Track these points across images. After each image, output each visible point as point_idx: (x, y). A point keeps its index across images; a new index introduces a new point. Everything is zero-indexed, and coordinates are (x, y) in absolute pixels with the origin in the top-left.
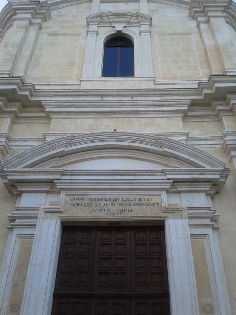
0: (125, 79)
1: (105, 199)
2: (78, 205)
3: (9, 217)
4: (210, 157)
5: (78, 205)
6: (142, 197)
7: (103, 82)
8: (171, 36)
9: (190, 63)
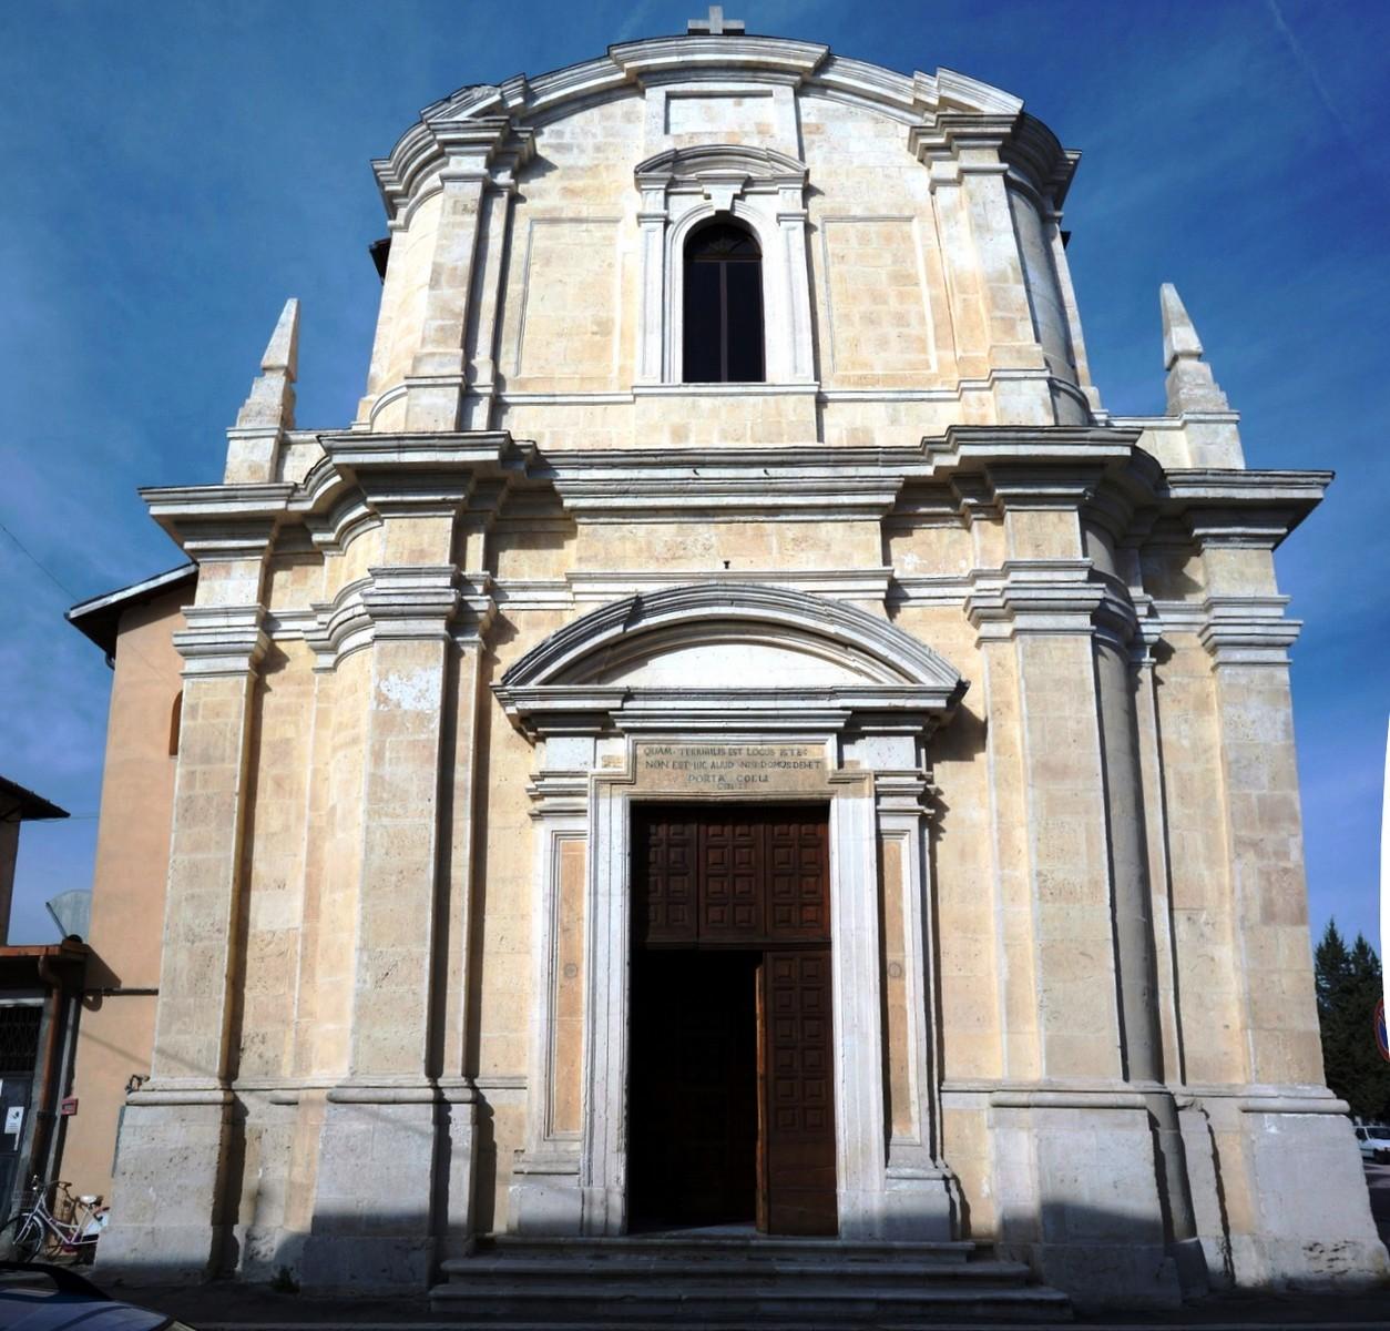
1: (712, 752)
2: (660, 764)
3: (529, 790)
4: (932, 656)
5: (660, 764)
6: (786, 747)
7: (691, 399)
9: (908, 325)
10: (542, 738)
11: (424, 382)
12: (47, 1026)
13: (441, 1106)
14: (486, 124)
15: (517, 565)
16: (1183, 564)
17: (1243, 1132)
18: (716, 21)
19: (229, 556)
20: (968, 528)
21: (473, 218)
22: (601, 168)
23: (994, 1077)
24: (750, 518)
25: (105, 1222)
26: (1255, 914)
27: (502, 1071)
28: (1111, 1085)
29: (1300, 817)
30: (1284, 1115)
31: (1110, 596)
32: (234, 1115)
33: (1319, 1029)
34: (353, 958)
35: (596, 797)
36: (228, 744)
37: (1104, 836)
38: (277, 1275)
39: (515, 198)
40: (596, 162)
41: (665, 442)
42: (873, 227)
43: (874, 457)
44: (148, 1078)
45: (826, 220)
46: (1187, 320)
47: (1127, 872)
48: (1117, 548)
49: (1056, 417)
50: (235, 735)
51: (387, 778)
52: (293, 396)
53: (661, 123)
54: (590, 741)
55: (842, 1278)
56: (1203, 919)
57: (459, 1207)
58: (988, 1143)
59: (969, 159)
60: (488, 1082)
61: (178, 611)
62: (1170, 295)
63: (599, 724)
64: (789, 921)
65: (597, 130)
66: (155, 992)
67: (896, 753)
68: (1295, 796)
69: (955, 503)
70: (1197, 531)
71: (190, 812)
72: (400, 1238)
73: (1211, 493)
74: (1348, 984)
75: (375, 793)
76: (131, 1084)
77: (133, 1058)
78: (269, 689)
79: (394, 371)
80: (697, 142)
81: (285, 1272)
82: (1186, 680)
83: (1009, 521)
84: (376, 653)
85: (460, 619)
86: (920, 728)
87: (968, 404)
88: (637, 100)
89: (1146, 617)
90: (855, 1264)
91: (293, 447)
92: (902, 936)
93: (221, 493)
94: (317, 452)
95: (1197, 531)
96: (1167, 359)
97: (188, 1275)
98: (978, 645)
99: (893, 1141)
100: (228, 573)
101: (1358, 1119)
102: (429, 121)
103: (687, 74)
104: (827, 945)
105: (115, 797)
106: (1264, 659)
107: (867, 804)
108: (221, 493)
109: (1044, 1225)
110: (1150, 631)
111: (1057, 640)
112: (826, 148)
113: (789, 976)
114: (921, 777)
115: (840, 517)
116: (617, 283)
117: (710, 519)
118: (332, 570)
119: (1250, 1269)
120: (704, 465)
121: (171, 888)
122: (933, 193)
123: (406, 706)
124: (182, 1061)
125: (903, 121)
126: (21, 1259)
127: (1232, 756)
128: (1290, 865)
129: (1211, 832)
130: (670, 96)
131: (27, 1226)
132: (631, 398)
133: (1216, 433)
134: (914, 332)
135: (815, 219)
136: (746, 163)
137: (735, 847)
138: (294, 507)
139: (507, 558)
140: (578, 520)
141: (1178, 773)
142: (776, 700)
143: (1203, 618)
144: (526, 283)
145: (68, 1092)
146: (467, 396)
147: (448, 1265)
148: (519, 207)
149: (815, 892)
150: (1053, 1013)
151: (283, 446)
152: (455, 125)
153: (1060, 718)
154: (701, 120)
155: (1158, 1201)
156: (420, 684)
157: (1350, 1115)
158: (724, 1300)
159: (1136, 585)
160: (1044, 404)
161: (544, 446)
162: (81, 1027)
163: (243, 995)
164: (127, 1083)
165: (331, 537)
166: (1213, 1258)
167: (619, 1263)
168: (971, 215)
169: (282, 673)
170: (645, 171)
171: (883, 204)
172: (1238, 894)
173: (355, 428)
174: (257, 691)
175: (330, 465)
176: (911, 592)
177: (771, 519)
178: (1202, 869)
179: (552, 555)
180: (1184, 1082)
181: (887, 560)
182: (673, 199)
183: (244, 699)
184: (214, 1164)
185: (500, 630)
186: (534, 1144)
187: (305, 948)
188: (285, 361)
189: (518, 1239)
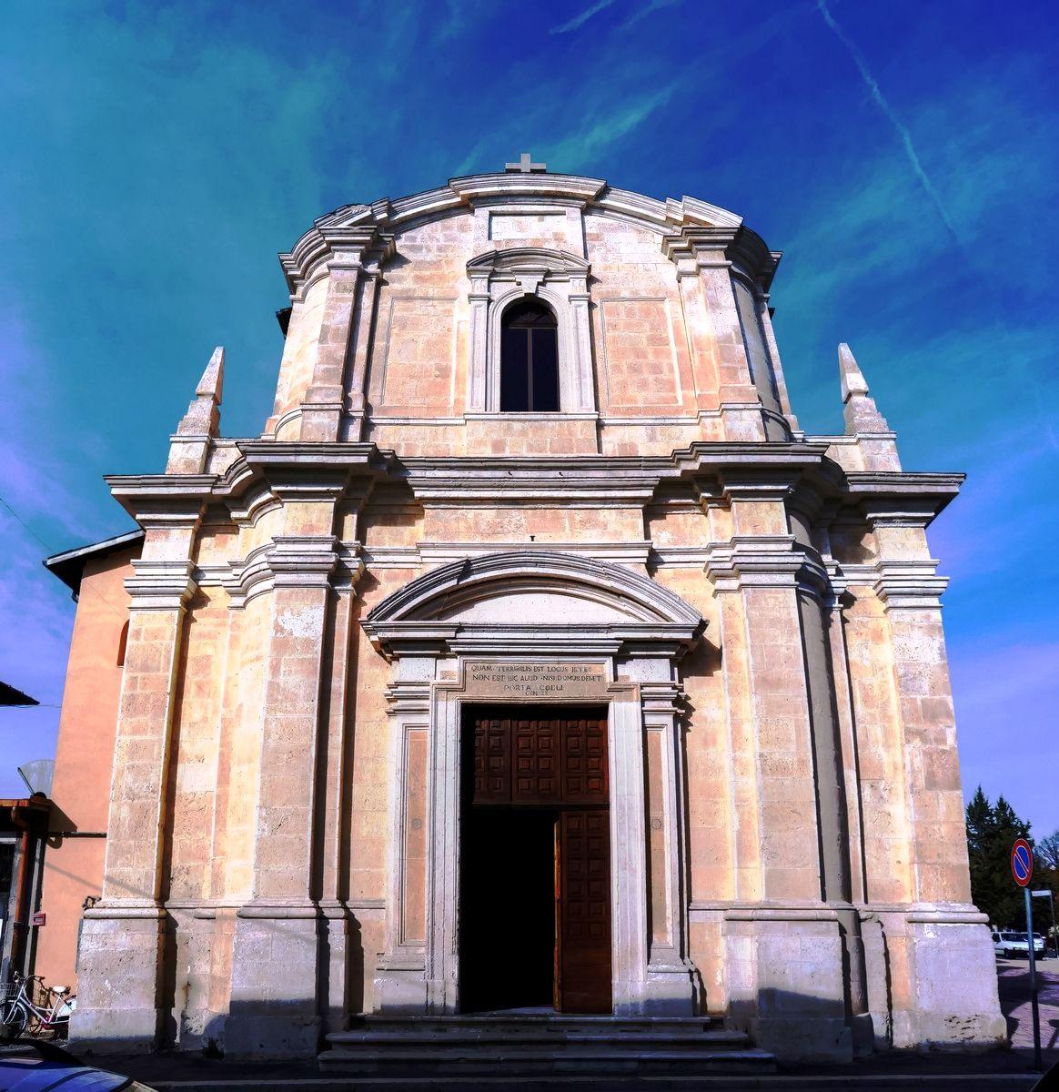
0: (545, 417)
1: (522, 669)
2: (484, 677)
3: (386, 695)
5: (484, 677)
7: (505, 423)
8: (627, 303)
10: (396, 658)
11: (314, 407)
12: (18, 859)
13: (322, 921)
14: (360, 231)
15: (380, 537)
16: (860, 538)
17: (909, 937)
18: (526, 163)
19: (168, 525)
20: (706, 514)
21: (351, 295)
22: (443, 263)
23: (727, 899)
24: (549, 506)
25: (74, 1006)
26: (921, 782)
27: (366, 896)
28: (813, 904)
29: (953, 713)
30: (939, 924)
31: (809, 561)
32: (168, 928)
33: (968, 863)
34: (255, 813)
35: (436, 700)
36: (162, 658)
37: (809, 728)
38: (206, 1045)
39: (381, 283)
40: (438, 258)
41: (488, 452)
42: (637, 305)
43: (638, 464)
44: (100, 899)
45: (606, 299)
46: (857, 368)
47: (826, 754)
48: (812, 528)
49: (767, 436)
50: (169, 652)
51: (282, 685)
52: (219, 414)
53: (486, 233)
54: (432, 660)
55: (614, 1043)
56: (882, 787)
57: (337, 997)
58: (722, 947)
59: (704, 258)
60: (357, 904)
61: (129, 563)
62: (845, 351)
63: (440, 649)
64: (579, 789)
65: (440, 235)
66: (104, 836)
67: (657, 671)
68: (949, 700)
69: (696, 497)
70: (870, 515)
71: (132, 705)
72: (295, 1017)
73: (879, 488)
74: (991, 831)
75: (272, 695)
76: (87, 902)
77: (89, 884)
78: (195, 620)
79: (293, 398)
80: (511, 246)
81: (212, 1042)
82: (866, 620)
83: (735, 509)
84: (275, 597)
85: (338, 574)
86: (674, 653)
87: (704, 426)
88: (469, 216)
89: (835, 576)
90: (623, 1033)
91: (218, 449)
92: (661, 800)
93: (163, 481)
94: (234, 454)
95: (870, 515)
96: (844, 396)
97: (141, 1045)
98: (714, 596)
99: (653, 946)
100: (167, 537)
101: (995, 927)
102: (322, 227)
103: (504, 199)
104: (607, 807)
105: (75, 694)
106: (923, 604)
107: (635, 707)
108: (163, 481)
109: (759, 1004)
110: (838, 585)
111: (771, 592)
112: (603, 250)
113: (579, 829)
114: (674, 687)
115: (614, 506)
116: (454, 342)
117: (520, 507)
118: (246, 537)
119: (904, 1037)
120: (515, 468)
121: (117, 763)
122: (679, 282)
123: (296, 634)
124: (127, 887)
125: (658, 232)
126: (13, 1033)
127: (901, 672)
128: (946, 748)
129: (887, 726)
130: (492, 214)
131: (13, 1010)
132: (463, 422)
133: (880, 447)
134: (665, 377)
135: (596, 300)
136: (546, 260)
137: (538, 736)
138: (217, 492)
139: (373, 532)
140: (425, 506)
141: (860, 683)
142: (568, 632)
143: (876, 576)
144: (388, 341)
145: (38, 908)
146: (345, 418)
147: (331, 1037)
148: (383, 288)
149: (598, 769)
150: (771, 853)
151: (211, 449)
152: (338, 231)
153: (773, 646)
154: (512, 231)
155: (842, 986)
156: (307, 618)
157: (989, 924)
158: (531, 1061)
159: (826, 553)
160: (758, 427)
161: (401, 453)
162: (46, 860)
163: (172, 838)
164: (84, 902)
165: (245, 514)
166: (879, 1029)
167: (455, 1034)
168: (707, 296)
169: (205, 609)
170: (474, 266)
171: (643, 288)
172: (908, 768)
173: (263, 438)
174: (186, 622)
175: (244, 463)
176: (665, 558)
177: (564, 506)
178: (881, 750)
179: (406, 531)
180: (866, 902)
181: (647, 536)
182: (493, 284)
183: (176, 627)
184: (154, 963)
185: (367, 582)
186: (391, 948)
187: (218, 805)
188: (213, 390)
189: (381, 1018)
